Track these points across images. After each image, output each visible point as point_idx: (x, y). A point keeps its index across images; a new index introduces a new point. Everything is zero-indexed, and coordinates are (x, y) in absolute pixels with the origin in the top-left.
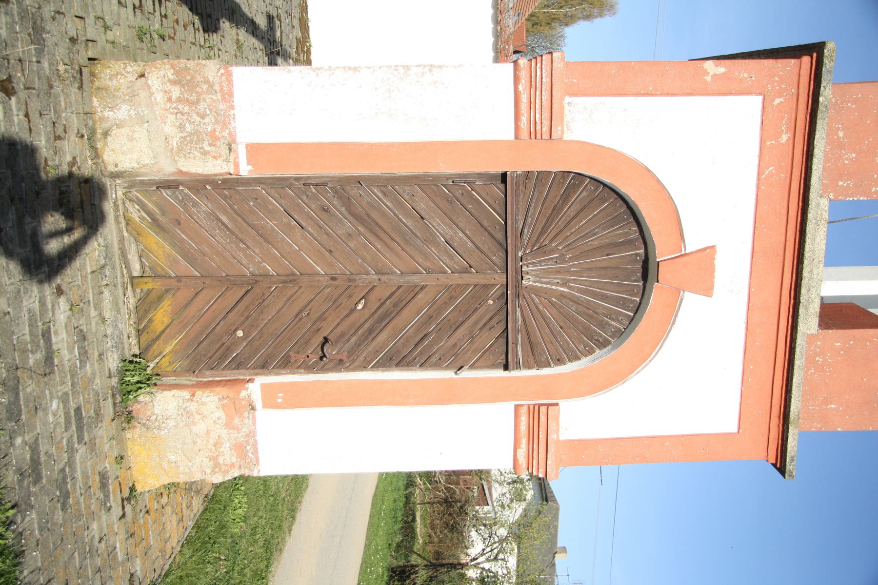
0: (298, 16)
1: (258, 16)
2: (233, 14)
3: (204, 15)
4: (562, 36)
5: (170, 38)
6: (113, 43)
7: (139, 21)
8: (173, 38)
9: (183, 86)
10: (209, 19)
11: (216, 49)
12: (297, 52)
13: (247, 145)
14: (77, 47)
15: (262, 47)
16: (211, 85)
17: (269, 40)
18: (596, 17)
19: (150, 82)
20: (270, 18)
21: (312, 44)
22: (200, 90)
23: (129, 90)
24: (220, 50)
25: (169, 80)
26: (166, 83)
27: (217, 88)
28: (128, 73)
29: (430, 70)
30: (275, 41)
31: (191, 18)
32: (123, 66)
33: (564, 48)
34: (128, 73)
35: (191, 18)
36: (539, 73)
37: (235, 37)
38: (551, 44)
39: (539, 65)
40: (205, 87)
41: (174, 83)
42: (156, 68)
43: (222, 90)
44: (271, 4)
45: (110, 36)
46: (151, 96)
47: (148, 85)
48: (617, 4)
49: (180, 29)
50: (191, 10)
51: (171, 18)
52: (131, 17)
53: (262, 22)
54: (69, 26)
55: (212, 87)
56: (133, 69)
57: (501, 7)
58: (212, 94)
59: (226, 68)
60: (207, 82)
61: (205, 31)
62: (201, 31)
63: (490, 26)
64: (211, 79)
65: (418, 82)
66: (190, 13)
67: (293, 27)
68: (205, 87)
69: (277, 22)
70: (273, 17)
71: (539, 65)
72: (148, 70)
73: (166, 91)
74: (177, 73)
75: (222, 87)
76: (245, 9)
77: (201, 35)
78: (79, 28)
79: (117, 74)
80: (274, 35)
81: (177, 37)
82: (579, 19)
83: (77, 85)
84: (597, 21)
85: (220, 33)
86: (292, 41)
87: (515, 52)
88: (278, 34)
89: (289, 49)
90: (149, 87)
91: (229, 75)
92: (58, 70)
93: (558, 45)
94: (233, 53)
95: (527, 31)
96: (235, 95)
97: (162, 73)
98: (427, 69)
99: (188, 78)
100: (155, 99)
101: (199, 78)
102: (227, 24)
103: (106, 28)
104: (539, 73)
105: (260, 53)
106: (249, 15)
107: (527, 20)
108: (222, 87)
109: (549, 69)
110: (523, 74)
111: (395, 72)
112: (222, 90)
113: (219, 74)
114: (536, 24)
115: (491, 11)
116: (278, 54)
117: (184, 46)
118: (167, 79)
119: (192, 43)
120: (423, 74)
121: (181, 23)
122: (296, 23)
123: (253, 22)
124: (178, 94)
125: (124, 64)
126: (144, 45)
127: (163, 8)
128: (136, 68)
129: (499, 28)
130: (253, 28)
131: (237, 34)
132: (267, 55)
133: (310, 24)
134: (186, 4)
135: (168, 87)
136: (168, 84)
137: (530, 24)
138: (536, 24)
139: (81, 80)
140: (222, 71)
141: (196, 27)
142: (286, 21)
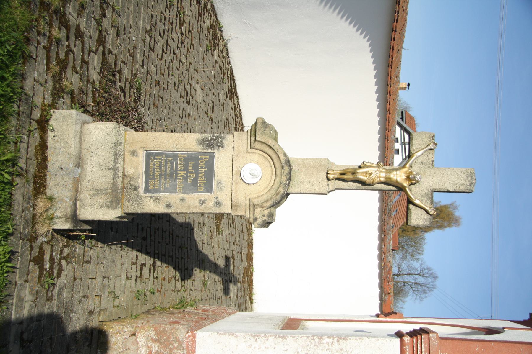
0: (246, 253)
1: (219, 260)
2: (202, 263)
3: (183, 269)
4: (422, 238)
5: (158, 291)
6: (118, 306)
7: (139, 286)
8: (160, 291)
9: (161, 343)
10: (186, 271)
11: (188, 290)
12: (244, 277)
13: (211, 193)
14: (93, 316)
15: (220, 279)
16: (180, 344)
17: (225, 273)
18: (446, 227)
19: (138, 340)
20: (227, 259)
21: (254, 270)
22: (172, 347)
23: (123, 345)
24: (191, 290)
25: (152, 339)
26: (149, 341)
27: (185, 346)
28: (124, 332)
29: (338, 341)
30: (229, 273)
31: (174, 274)
32: (121, 327)
33: (424, 247)
34: (124, 332)
35: (174, 274)
36: (419, 348)
37: (202, 278)
38: (415, 243)
39: (419, 342)
40: (176, 345)
41: (155, 341)
42: (144, 330)
43: (187, 348)
44: (228, 250)
45: (117, 302)
46: (138, 349)
47: (137, 342)
48: (460, 219)
49: (165, 283)
50: (174, 268)
51: (160, 277)
52: (133, 285)
53: (221, 263)
54: (90, 304)
55: (181, 345)
56: (128, 329)
57: (384, 249)
58: (180, 350)
59: (192, 332)
60: (178, 341)
61: (182, 280)
62: (180, 280)
63: (377, 262)
64: (181, 339)
65: (329, 349)
66: (174, 271)
67: (242, 261)
68: (176, 345)
69: (232, 260)
70: (229, 258)
71: (419, 342)
72: (138, 331)
73: (148, 347)
74: (157, 334)
75: (188, 345)
76: (211, 258)
77: (179, 284)
78: (97, 303)
79: (117, 333)
80: (229, 269)
81: (163, 290)
82: (434, 228)
83: (87, 344)
84: (447, 229)
85: (192, 278)
86: (241, 271)
87: (393, 250)
88: (232, 268)
89: (238, 276)
90: (137, 343)
91: (194, 337)
92: (77, 337)
93: (421, 244)
94: (200, 289)
95: (399, 235)
96: (196, 351)
97: (147, 333)
98: (336, 339)
99: (165, 338)
100: (140, 352)
101: (172, 338)
102: (198, 270)
103: (115, 297)
104: (419, 348)
105: (218, 284)
106: (213, 260)
107: (400, 228)
108: (188, 345)
109: (427, 345)
110: (407, 348)
111: (312, 341)
112: (187, 348)
113: (187, 336)
114: (405, 230)
115: (377, 252)
116: (231, 282)
117: (167, 294)
118: (150, 338)
119: (173, 291)
120: (332, 344)
121: (167, 279)
122: (244, 258)
123: (216, 265)
124: (156, 349)
125: (123, 325)
126: (139, 302)
127: (156, 272)
128: (130, 329)
129: (383, 264)
130: (214, 268)
131: (204, 276)
132: (223, 284)
133: (254, 257)
134: (172, 265)
135: (151, 343)
136: (151, 341)
137: (400, 231)
138: (405, 230)
139: (91, 339)
140: (189, 334)
141: (177, 279)
142: (237, 257)
